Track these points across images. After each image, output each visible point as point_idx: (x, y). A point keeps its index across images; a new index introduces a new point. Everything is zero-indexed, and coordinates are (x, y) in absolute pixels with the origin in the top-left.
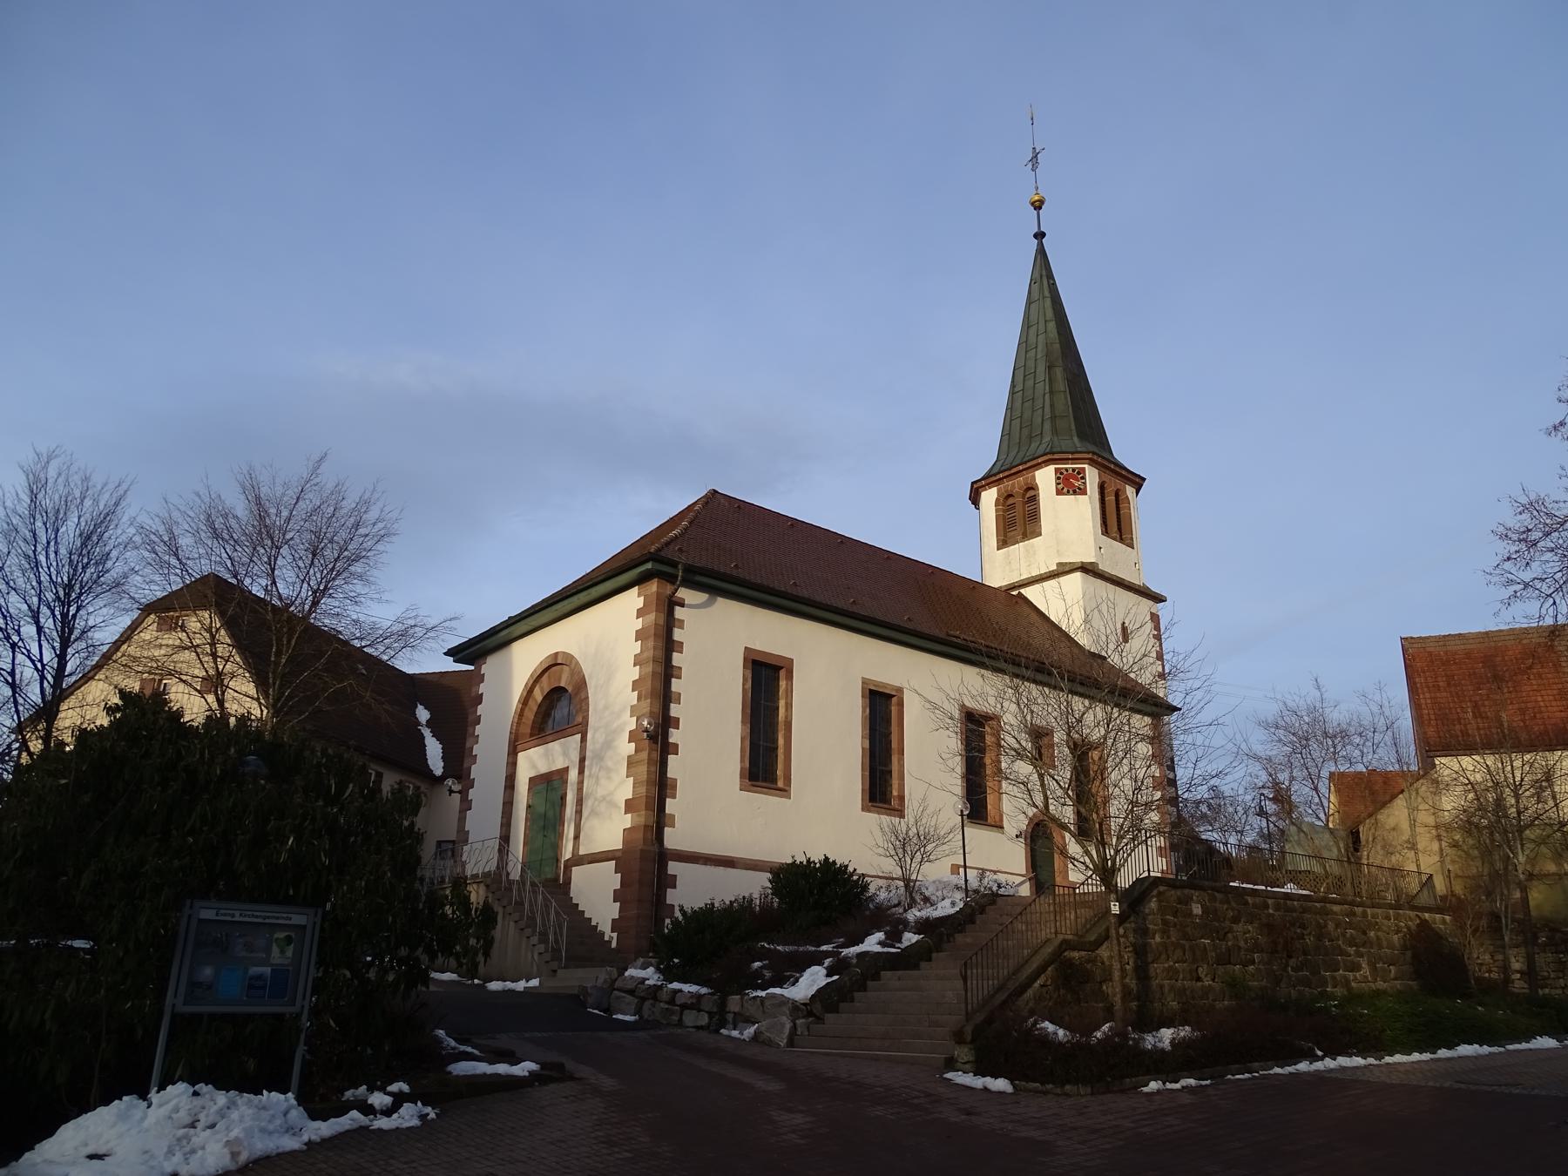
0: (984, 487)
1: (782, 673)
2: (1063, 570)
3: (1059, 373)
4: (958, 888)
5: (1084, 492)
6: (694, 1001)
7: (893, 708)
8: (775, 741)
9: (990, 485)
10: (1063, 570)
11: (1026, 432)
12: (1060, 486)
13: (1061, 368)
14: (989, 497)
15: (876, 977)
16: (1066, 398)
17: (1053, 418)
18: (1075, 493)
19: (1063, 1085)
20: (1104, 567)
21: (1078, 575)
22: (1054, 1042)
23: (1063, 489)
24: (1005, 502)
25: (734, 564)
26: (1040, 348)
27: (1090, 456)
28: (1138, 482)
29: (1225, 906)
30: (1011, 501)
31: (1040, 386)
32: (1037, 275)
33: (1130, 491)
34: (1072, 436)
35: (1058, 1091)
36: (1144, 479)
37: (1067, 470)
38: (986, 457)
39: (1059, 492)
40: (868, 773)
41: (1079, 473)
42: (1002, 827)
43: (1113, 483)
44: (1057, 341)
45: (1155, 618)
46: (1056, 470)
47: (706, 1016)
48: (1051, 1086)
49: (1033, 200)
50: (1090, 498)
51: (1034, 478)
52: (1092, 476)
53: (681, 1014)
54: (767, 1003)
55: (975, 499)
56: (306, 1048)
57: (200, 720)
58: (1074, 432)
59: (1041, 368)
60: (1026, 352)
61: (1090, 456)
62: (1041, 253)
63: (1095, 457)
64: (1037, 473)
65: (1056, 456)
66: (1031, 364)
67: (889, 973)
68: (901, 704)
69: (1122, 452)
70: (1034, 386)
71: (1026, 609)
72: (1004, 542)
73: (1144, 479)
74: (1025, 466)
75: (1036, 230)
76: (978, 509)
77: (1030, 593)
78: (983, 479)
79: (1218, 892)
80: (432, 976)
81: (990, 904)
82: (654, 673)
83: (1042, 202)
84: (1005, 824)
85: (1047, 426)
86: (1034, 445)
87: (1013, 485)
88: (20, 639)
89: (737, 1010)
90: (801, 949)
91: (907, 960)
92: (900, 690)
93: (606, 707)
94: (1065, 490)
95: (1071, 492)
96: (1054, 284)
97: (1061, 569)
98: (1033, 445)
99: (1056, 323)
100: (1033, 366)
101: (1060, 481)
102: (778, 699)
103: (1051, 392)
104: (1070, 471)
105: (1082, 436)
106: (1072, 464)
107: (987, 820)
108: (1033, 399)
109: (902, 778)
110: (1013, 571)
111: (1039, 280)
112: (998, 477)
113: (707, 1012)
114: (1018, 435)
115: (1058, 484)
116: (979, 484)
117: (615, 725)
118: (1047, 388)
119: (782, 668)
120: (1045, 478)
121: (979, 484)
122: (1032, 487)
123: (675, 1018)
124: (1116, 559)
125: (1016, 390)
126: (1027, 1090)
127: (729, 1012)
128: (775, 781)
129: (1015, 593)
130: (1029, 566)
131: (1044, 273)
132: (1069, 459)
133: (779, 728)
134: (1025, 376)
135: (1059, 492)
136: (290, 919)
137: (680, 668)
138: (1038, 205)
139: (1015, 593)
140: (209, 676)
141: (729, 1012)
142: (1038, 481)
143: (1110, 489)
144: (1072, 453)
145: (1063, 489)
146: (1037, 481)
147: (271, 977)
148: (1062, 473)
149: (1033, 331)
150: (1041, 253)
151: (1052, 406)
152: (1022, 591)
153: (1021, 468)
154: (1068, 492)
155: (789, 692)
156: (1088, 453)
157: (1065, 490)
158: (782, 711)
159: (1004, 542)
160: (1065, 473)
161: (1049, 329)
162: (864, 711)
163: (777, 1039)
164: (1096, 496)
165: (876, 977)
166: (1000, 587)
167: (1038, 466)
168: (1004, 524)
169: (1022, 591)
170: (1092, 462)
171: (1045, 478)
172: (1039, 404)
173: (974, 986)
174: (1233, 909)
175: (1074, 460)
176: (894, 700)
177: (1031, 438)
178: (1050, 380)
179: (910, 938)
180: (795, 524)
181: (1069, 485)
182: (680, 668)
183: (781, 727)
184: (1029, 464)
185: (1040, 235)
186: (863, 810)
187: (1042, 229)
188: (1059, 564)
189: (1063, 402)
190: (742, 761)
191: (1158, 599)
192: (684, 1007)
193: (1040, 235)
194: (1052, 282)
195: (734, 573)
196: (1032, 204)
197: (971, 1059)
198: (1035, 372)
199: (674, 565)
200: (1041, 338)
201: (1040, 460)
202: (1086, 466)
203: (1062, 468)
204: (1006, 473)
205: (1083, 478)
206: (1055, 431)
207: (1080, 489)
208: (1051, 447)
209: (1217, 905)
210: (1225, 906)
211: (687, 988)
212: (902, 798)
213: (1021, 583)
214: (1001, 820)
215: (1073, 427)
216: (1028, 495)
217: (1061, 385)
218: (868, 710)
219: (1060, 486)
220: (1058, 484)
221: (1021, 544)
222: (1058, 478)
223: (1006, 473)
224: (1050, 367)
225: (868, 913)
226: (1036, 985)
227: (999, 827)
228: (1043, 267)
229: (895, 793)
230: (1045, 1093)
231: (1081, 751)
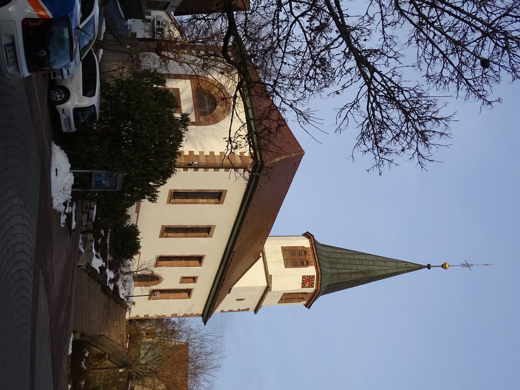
0: (311, 241)
1: (217, 200)
2: (268, 278)
3: (360, 276)
4: (129, 293)
5: (303, 286)
6: (90, 218)
7: (204, 234)
8: (190, 198)
9: (311, 244)
10: (268, 278)
11: (334, 260)
12: (306, 277)
13: (362, 277)
14: (306, 243)
15: (99, 283)
16: (347, 279)
17: (339, 274)
18: (303, 283)
19: (70, 368)
20: (269, 294)
21: (265, 284)
23: (305, 278)
24: (302, 251)
25: (262, 185)
26: (373, 267)
27: (319, 291)
28: (308, 305)
29: (122, 385)
30: (303, 253)
31: (355, 267)
32: (410, 265)
33: (305, 302)
34: (329, 282)
35: (69, 367)
36: (309, 308)
37: (313, 280)
39: (303, 277)
40: (177, 227)
41: (311, 285)
42: (156, 267)
43: (308, 298)
44: (375, 275)
45: (247, 310)
46: (314, 276)
47: (85, 224)
48: (70, 365)
49: (446, 264)
50: (301, 289)
51: (312, 265)
52: (311, 290)
53: (86, 213)
54: (91, 253)
55: (307, 235)
58: (331, 283)
59: (364, 268)
60: (373, 260)
61: (319, 291)
62: (420, 267)
63: (318, 292)
64: (314, 267)
65: (320, 277)
66: (367, 263)
67: (100, 288)
68: (205, 237)
69: (322, 299)
70: (355, 264)
72: (285, 250)
73: (309, 308)
74: (317, 262)
75: (431, 265)
76: (303, 236)
77: (261, 260)
78: (314, 239)
79: (127, 384)
81: (123, 307)
82: (216, 163)
83: (445, 268)
84: (157, 268)
85: (335, 271)
86: (327, 265)
87: (310, 255)
89: (88, 238)
90: (108, 252)
91: (105, 288)
92: (211, 237)
93: (204, 136)
94: (304, 279)
95: (303, 282)
96: (404, 273)
97: (269, 277)
98: (327, 264)
99: (385, 274)
100: (365, 264)
101: (309, 278)
102: (207, 199)
103: (351, 273)
104: (313, 282)
105: (329, 286)
106: (316, 283)
107: (159, 261)
108: (355, 259)
109: (175, 237)
110: (271, 254)
111: (407, 266)
112: (314, 248)
113: (87, 224)
114: (333, 256)
115: (307, 277)
116: (312, 239)
117: (196, 142)
118: (354, 271)
119: (219, 201)
121: (312, 239)
122: (307, 264)
123: (85, 210)
124: (271, 300)
125: (356, 256)
126: (69, 358)
127: (87, 235)
128: (173, 198)
129: (261, 255)
130: (272, 262)
131: (410, 269)
132: (318, 281)
133: (195, 200)
134: (361, 260)
135: (303, 277)
136: (118, 186)
137: (218, 171)
138: (444, 266)
139: (261, 255)
141: (87, 235)
142: (310, 267)
143: (304, 296)
144: (320, 283)
146: (310, 267)
147: (101, 108)
148: (312, 278)
149: (382, 263)
150: (420, 267)
151: (345, 273)
152: (261, 259)
153: (317, 260)
154: (304, 281)
155: (210, 203)
156: (320, 290)
157: (304, 279)
158: (201, 200)
159: (285, 250)
160: (312, 280)
161: (382, 271)
162: (202, 226)
163: (79, 262)
164: (301, 292)
165: (99, 283)
166: (264, 248)
167: (316, 268)
168: (292, 250)
169: (261, 259)
170: (316, 291)
171: (311, 271)
172: (346, 267)
174: (121, 387)
175: (317, 284)
176: (207, 234)
177: (331, 263)
178: (357, 272)
179: (112, 287)
180: (275, 217)
181: (306, 281)
182: (218, 171)
183: (195, 200)
184: (318, 264)
185: (429, 267)
186: (162, 226)
187: (432, 268)
188: (271, 276)
189: (346, 278)
190: (181, 190)
191: (256, 311)
192: (88, 214)
193: (429, 267)
194: (405, 272)
195: (258, 185)
196: (445, 264)
197: (77, 339)
198: (362, 265)
199: (260, 172)
200: (378, 268)
201: (319, 269)
202: (315, 288)
204: (315, 253)
205: (309, 287)
206: (332, 274)
208: (324, 274)
209: (123, 384)
210: (122, 385)
211: (95, 212)
212: (167, 237)
213: (265, 258)
214: (159, 266)
215: (334, 282)
216: (304, 261)
217: (354, 277)
218: (203, 227)
219: (306, 277)
221: (283, 258)
222: (310, 277)
223: (315, 253)
224: (363, 272)
226: (98, 350)
227: (156, 266)
228: (413, 268)
229: (169, 234)
230: (68, 364)
231: (189, 292)
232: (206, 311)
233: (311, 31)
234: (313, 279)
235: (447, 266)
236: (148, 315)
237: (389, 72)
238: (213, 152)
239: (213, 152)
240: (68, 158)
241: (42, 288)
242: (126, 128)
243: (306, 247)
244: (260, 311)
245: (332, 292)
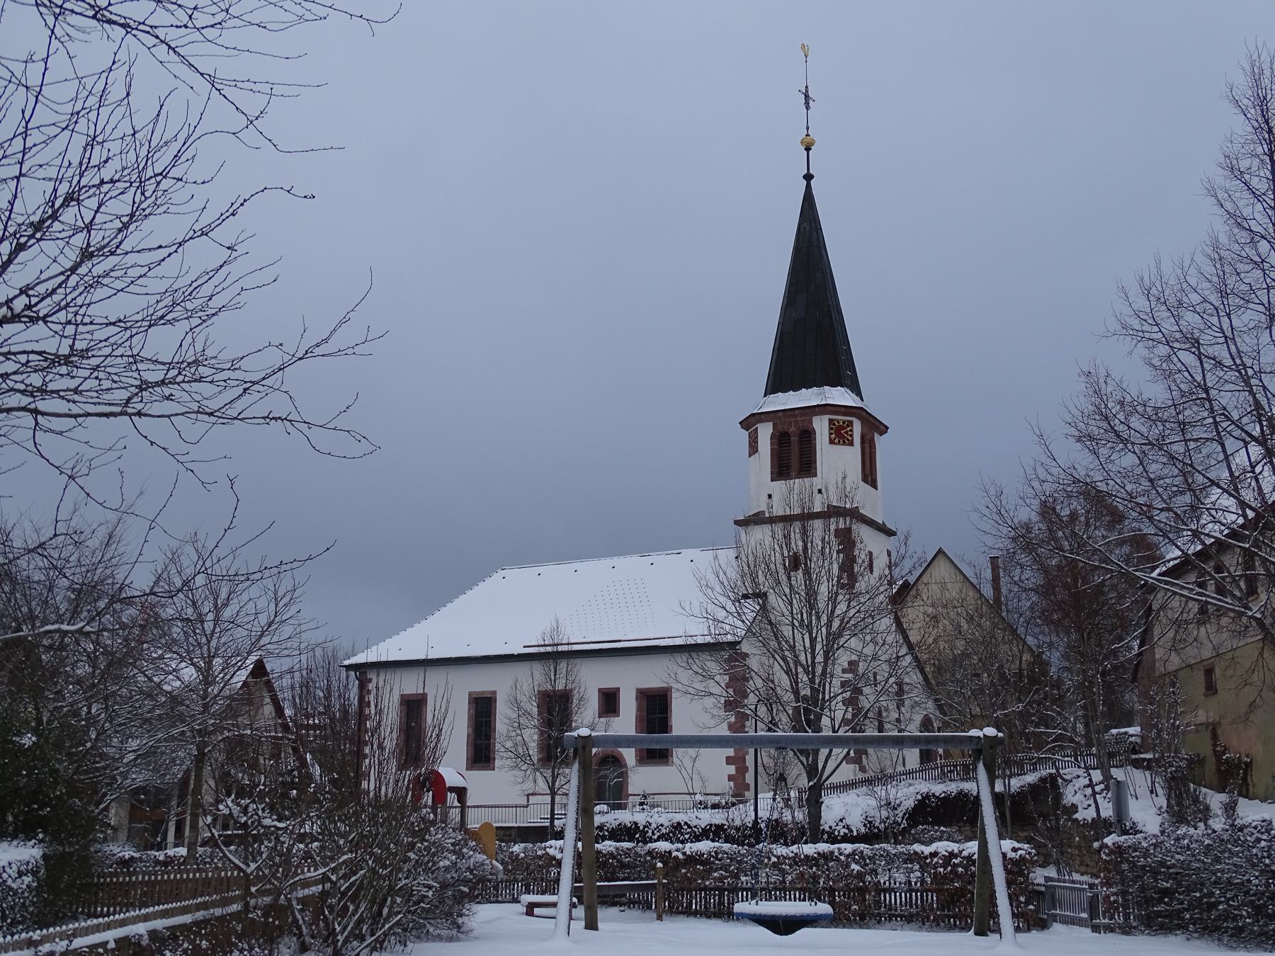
5: (851, 444)
22: (59, 924)
23: (835, 439)
28: (883, 429)
39: (832, 442)
46: (831, 421)
56: (855, 872)
62: (808, 199)
88: (125, 18)
94: (837, 440)
95: (841, 442)
101: (833, 431)
104: (841, 423)
115: (851, 430)
135: (832, 442)
145: (835, 439)
148: (834, 425)
150: (808, 199)
154: (839, 441)
157: (837, 440)
185: (809, 177)
193: (809, 177)
207: (848, 440)
219: (833, 436)
220: (832, 434)
222: (831, 429)
225: (248, 899)
233: (1201, 825)
235: (808, 139)
237: (169, 417)
238: (729, 776)
239: (729, 776)
240: (786, 391)
243: (771, 430)
244: (890, 526)
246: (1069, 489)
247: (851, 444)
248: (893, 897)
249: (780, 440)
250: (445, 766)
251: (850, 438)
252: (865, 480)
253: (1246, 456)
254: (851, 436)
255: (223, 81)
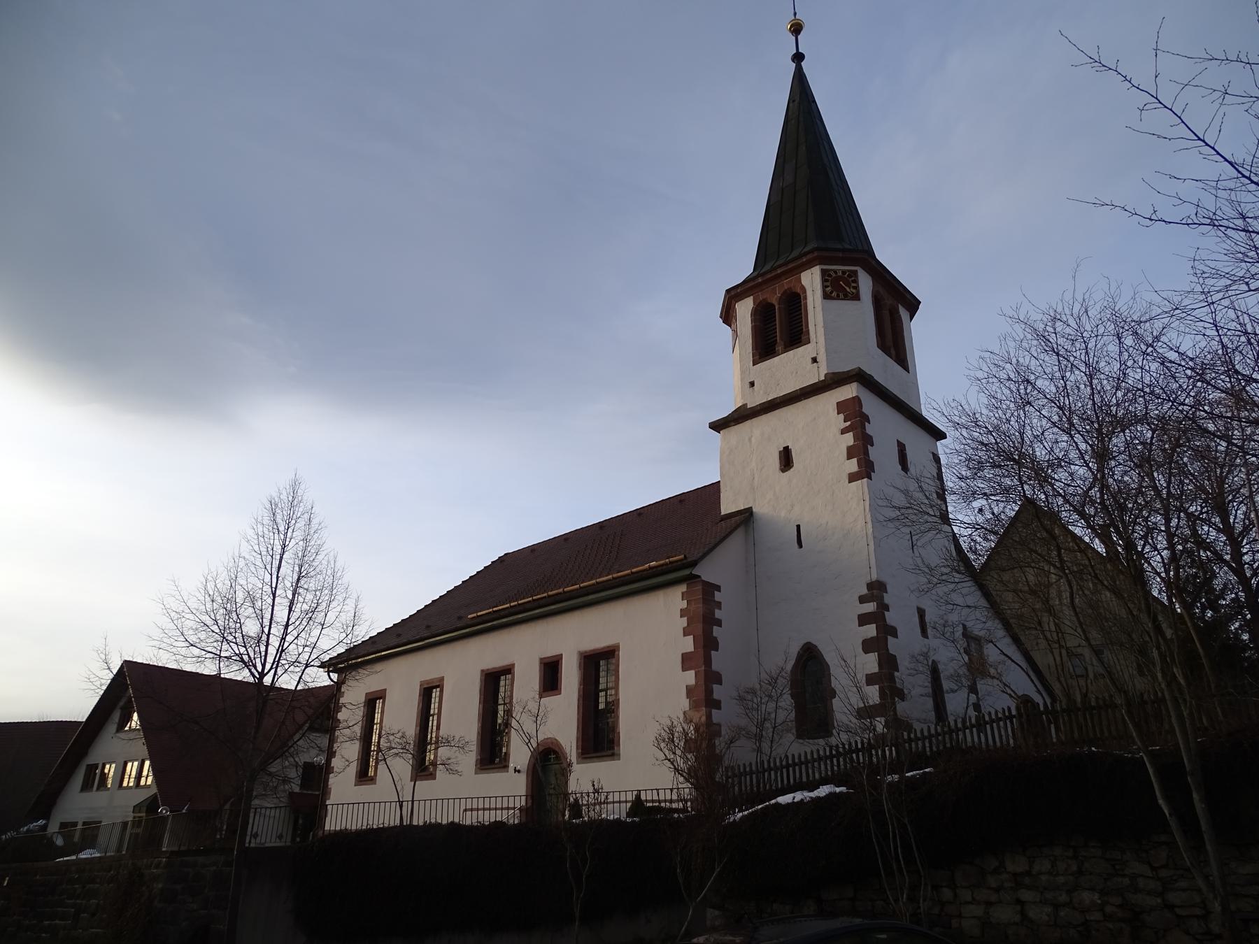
5: (856, 297)
12: (829, 289)
14: (745, 309)
23: (831, 293)
33: (904, 313)
37: (835, 272)
38: (742, 266)
46: (824, 272)
57: (687, 789)
62: (800, 80)
71: (790, 113)
80: (1012, 745)
94: (834, 294)
101: (828, 284)
104: (840, 274)
120: (811, 280)
135: (826, 296)
137: (508, 772)
140: (293, 757)
145: (831, 293)
150: (800, 80)
154: (838, 296)
157: (834, 294)
160: (834, 275)
173: (748, 783)
185: (798, 57)
193: (798, 57)
203: (832, 270)
219: (829, 289)
220: (827, 287)
232: (1037, 684)
234: (832, 273)
236: (717, 650)
241: (1066, 688)
242: (1234, 565)
245: (814, 101)
246: (1223, 576)
247: (856, 297)
248: (804, 770)
249: (763, 317)
250: (868, 481)
251: (854, 291)
252: (882, 346)
253: (1016, 666)
254: (856, 288)
255: (277, 660)
